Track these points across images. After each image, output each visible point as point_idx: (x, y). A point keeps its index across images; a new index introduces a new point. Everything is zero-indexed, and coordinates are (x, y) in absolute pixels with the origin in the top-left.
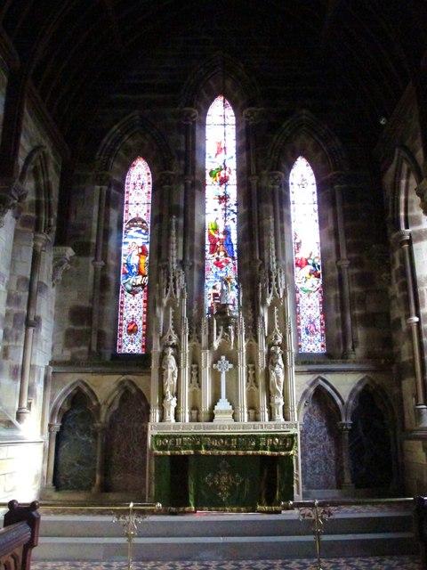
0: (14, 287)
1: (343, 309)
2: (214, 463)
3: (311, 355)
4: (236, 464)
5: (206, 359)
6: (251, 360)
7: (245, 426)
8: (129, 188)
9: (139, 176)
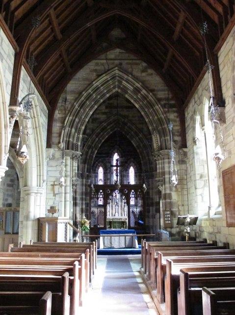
0: (47, 212)
1: (82, 200)
2: (115, 222)
3: (100, 205)
4: (119, 222)
5: (114, 206)
6: (121, 206)
7: (120, 217)
8: (99, 173)
9: (101, 171)
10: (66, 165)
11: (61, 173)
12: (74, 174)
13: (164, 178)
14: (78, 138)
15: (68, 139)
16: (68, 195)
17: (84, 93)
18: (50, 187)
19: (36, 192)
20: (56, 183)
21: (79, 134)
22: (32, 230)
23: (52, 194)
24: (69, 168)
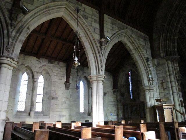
9: (82, 85)
10: (168, 67)
11: (166, 74)
12: (176, 72)
13: (50, 91)
14: (174, 47)
15: (165, 49)
16: (174, 88)
17: (170, 35)
18: (160, 85)
19: (148, 89)
20: (164, 81)
21: (173, 43)
22: (150, 114)
23: (163, 89)
24: (171, 69)
